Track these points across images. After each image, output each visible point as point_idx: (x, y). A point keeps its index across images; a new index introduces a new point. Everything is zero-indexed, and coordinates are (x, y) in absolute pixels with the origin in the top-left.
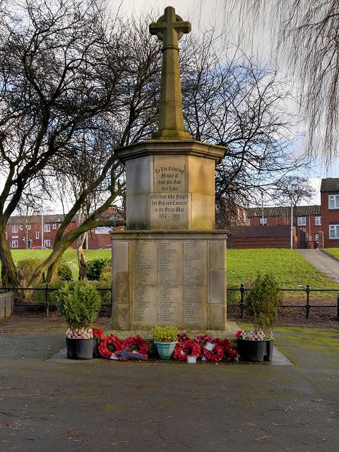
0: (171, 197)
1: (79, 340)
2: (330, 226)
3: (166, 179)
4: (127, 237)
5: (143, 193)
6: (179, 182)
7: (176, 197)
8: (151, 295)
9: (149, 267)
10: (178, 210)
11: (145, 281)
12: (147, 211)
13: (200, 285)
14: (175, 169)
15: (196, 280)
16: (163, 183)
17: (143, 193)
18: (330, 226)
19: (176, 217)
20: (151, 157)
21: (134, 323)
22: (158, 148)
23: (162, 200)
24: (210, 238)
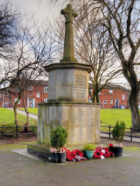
0: (80, 88)
1: (63, 153)
2: (44, 99)
3: (79, 80)
4: (68, 105)
5: (68, 85)
8: (76, 130)
9: (76, 118)
10: (83, 94)
11: (74, 125)
12: (71, 93)
13: (93, 126)
14: (82, 76)
15: (92, 124)
16: (78, 81)
17: (68, 85)
18: (44, 99)
19: (82, 96)
21: (70, 143)
22: (84, 67)
23: (78, 89)
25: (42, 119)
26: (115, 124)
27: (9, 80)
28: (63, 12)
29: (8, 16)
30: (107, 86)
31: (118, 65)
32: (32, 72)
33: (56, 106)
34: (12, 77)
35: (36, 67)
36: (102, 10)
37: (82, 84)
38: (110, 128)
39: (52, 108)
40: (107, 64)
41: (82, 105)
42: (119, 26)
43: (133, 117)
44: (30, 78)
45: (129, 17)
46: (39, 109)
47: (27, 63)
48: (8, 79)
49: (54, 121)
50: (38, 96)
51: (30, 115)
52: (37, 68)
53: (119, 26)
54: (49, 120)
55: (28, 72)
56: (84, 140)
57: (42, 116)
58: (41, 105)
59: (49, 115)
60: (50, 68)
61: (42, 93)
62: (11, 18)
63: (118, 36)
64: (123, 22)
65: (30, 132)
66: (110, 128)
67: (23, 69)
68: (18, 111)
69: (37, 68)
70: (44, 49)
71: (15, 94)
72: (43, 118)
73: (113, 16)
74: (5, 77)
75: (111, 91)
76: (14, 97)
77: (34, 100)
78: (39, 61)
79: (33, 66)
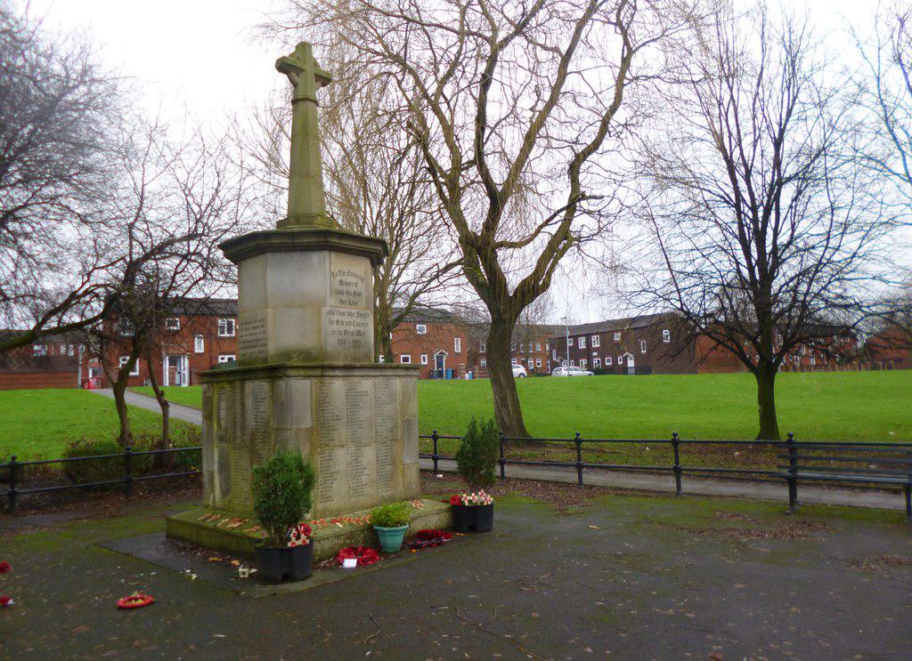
2: (220, 357)
4: (310, 373)
6: (360, 294)
7: (356, 315)
8: (342, 457)
9: (338, 418)
13: (394, 440)
18: (220, 357)
20: (327, 253)
21: (320, 506)
24: (402, 374)
25: (219, 422)
26: (466, 431)
27: (97, 295)
28: (283, 66)
29: (93, 81)
30: (414, 312)
31: (447, 247)
32: (176, 269)
33: (268, 380)
34: (108, 285)
35: (192, 250)
36: (399, 83)
37: (355, 303)
38: (435, 441)
39: (257, 388)
40: (411, 248)
41: (356, 373)
42: (448, 130)
43: (314, 388)
44: (171, 287)
45: (481, 104)
46: (205, 393)
47: (159, 236)
48: (92, 291)
49: (262, 430)
50: (199, 347)
51: (174, 411)
52: (194, 253)
53: (448, 130)
54: (243, 427)
55: (163, 267)
56: (367, 490)
57: (219, 416)
58: (208, 375)
59: (243, 412)
60: (244, 249)
61: (210, 338)
62: (102, 88)
63: (445, 163)
64: (458, 120)
65: (175, 467)
66: (435, 441)
67: (146, 257)
68: (130, 397)
69: (194, 253)
70: (217, 191)
71: (120, 342)
72: (223, 423)
73: (430, 101)
74: (81, 285)
75: (422, 329)
76: (117, 351)
77: (185, 363)
78: (200, 231)
79: (181, 248)
